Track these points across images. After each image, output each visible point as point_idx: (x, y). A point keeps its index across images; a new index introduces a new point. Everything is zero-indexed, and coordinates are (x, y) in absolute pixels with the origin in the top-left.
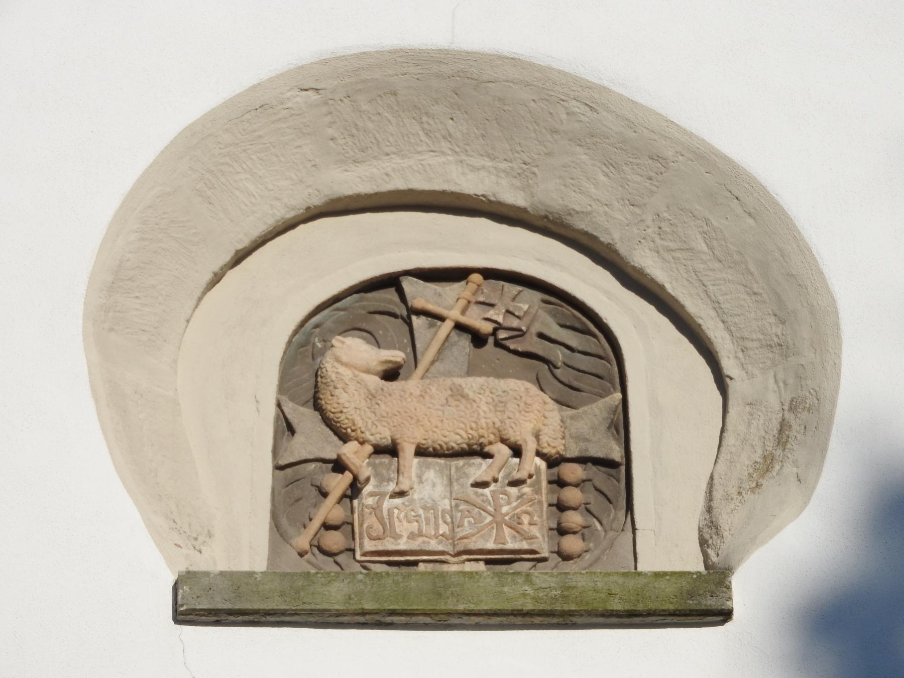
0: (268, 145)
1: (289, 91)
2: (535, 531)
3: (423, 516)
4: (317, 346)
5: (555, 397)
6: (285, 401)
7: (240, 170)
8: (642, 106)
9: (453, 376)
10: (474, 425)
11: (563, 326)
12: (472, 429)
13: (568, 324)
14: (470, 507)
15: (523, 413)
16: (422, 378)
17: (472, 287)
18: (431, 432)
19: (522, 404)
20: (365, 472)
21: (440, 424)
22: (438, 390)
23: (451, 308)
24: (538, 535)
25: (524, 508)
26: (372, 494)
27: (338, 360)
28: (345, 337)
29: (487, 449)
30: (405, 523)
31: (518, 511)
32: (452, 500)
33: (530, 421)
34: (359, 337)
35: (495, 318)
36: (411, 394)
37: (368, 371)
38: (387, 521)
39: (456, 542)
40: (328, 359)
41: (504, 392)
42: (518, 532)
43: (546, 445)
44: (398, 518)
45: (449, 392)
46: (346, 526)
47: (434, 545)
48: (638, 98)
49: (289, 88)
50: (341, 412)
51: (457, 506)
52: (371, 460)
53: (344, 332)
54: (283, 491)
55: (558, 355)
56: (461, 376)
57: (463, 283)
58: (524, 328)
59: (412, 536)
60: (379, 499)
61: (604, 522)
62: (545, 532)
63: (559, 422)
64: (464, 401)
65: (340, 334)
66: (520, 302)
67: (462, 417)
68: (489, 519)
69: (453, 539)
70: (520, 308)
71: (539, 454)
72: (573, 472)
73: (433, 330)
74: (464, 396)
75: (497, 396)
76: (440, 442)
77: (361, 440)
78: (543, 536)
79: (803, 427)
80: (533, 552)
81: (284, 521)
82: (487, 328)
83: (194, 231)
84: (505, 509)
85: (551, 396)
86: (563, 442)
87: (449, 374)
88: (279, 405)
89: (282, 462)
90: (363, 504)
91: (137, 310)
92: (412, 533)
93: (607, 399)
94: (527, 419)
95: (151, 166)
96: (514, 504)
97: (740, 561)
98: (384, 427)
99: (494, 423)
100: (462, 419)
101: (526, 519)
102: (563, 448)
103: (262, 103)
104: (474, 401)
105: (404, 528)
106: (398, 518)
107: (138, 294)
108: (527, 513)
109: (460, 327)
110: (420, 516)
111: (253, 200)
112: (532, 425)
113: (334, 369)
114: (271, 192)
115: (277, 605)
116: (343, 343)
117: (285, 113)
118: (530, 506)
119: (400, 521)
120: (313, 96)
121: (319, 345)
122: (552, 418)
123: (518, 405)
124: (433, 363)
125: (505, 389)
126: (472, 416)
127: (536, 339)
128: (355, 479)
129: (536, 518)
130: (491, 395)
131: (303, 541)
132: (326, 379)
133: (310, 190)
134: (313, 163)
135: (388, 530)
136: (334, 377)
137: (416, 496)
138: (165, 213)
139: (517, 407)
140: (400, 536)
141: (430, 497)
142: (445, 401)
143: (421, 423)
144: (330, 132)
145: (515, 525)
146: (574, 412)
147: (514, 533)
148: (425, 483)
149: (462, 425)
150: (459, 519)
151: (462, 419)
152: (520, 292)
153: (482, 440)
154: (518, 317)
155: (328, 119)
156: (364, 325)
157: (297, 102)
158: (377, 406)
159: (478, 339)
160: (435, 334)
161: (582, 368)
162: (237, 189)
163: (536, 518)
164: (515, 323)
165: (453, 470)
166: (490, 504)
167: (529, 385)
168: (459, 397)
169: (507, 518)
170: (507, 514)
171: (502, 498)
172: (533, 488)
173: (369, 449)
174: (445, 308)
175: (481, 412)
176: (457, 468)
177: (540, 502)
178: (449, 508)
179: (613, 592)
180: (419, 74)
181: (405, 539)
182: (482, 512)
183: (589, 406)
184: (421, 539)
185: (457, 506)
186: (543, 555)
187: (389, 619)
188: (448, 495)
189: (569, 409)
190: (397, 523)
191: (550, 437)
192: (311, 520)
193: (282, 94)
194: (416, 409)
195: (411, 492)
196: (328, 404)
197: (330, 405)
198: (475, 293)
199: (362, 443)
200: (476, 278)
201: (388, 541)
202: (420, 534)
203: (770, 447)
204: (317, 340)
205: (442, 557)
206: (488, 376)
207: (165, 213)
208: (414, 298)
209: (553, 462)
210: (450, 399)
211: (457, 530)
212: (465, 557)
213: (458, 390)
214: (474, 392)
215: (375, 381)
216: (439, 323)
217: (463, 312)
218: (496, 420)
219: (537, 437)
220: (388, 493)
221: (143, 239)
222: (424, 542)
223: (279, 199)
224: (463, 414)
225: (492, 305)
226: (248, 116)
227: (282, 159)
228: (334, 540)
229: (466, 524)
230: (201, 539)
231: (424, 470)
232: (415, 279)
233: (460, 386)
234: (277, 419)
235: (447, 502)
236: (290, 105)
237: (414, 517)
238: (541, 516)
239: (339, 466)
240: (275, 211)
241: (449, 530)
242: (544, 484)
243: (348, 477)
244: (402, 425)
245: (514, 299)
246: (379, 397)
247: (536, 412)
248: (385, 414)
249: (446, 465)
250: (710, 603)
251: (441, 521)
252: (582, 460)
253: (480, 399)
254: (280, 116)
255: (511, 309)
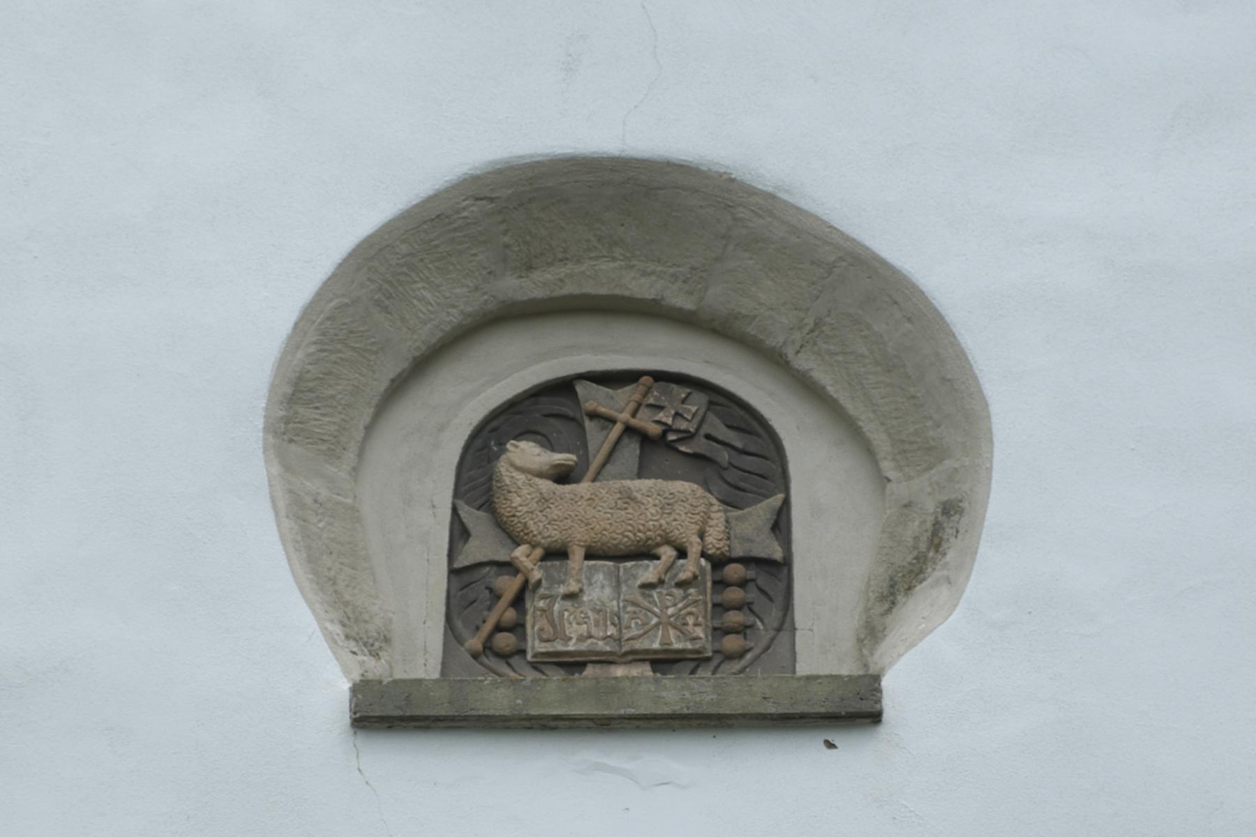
0: (445, 254)
1: (464, 200)
2: (699, 632)
3: (592, 618)
4: (494, 450)
5: (721, 498)
6: (461, 504)
7: (417, 279)
8: (806, 212)
9: (624, 479)
10: (641, 527)
11: (729, 427)
12: (639, 531)
13: (735, 425)
14: (637, 609)
15: (690, 515)
16: (594, 480)
17: (641, 389)
18: (600, 535)
19: (688, 506)
20: (537, 575)
21: (608, 526)
22: (608, 489)
23: (622, 411)
24: (702, 635)
25: (689, 609)
26: (543, 597)
27: (512, 465)
28: (518, 441)
29: (654, 552)
30: (574, 625)
31: (683, 612)
32: (620, 601)
33: (696, 523)
34: (534, 441)
35: (664, 420)
36: (582, 497)
37: (541, 475)
38: (557, 623)
39: (623, 643)
40: (503, 464)
41: (671, 494)
42: (682, 633)
43: (710, 546)
44: (568, 620)
45: (618, 495)
46: (518, 628)
47: (602, 646)
48: (804, 204)
49: (463, 197)
50: (514, 516)
51: (625, 607)
52: (544, 563)
53: (518, 437)
54: (460, 593)
55: (724, 456)
56: (632, 479)
57: (634, 386)
58: (692, 430)
59: (581, 639)
60: (550, 601)
61: (766, 621)
62: (709, 632)
63: (724, 523)
64: (632, 503)
65: (514, 439)
66: (690, 404)
67: (630, 519)
68: (655, 620)
69: (620, 640)
70: (689, 410)
71: (703, 555)
72: (734, 571)
73: (605, 432)
74: (634, 499)
75: (665, 498)
76: (609, 545)
77: (533, 543)
78: (707, 636)
79: (955, 530)
80: (697, 652)
81: (459, 624)
82: (654, 430)
83: (373, 340)
84: (670, 611)
85: (718, 496)
86: (728, 542)
87: (621, 476)
88: (455, 510)
89: (456, 565)
90: (535, 607)
91: (316, 420)
92: (581, 635)
93: (771, 500)
94: (692, 521)
95: (329, 279)
96: (680, 605)
97: (891, 664)
98: (555, 530)
99: (661, 525)
100: (631, 522)
101: (690, 620)
102: (727, 548)
103: (439, 213)
104: (643, 504)
105: (574, 630)
106: (568, 620)
107: (317, 405)
108: (690, 613)
109: (629, 430)
110: (588, 618)
111: (430, 308)
112: (698, 527)
113: (508, 473)
114: (449, 300)
115: (446, 712)
116: (517, 447)
117: (460, 222)
118: (695, 607)
119: (570, 623)
120: (490, 206)
121: (495, 449)
122: (718, 519)
123: (685, 507)
124: (604, 465)
125: (672, 491)
126: (639, 519)
127: (704, 440)
128: (526, 582)
129: (700, 619)
130: (659, 497)
131: (475, 642)
132: (501, 483)
133: (486, 297)
134: (488, 270)
135: (559, 633)
136: (507, 481)
137: (585, 598)
138: (344, 324)
139: (682, 508)
140: (570, 639)
141: (599, 599)
142: (614, 504)
143: (591, 526)
144: (506, 239)
145: (681, 628)
146: (740, 512)
147: (679, 633)
148: (595, 585)
149: (630, 528)
150: (626, 621)
151: (631, 522)
152: (689, 394)
153: (650, 542)
154: (687, 420)
155: (503, 227)
156: (539, 428)
157: (473, 211)
158: (548, 510)
159: (645, 439)
160: (608, 435)
161: (747, 468)
162: (415, 298)
163: (700, 619)
164: (683, 425)
165: (622, 570)
166: (656, 605)
167: (695, 486)
168: (628, 500)
169: (672, 619)
170: (672, 616)
171: (668, 599)
172: (697, 590)
173: (539, 552)
174: (617, 410)
175: (649, 514)
176: (625, 569)
177: (705, 603)
178: (616, 609)
179: (767, 696)
180: (591, 181)
181: (574, 641)
182: (649, 614)
183: (754, 507)
184: (589, 641)
185: (625, 607)
186: (706, 655)
187: (553, 724)
188: (616, 595)
189: (734, 509)
190: (567, 625)
191: (715, 539)
192: (484, 622)
193: (458, 203)
194: (586, 512)
195: (580, 594)
196: (502, 508)
197: (504, 510)
198: (645, 395)
199: (534, 547)
200: (646, 380)
201: (558, 643)
202: (590, 637)
203: (923, 546)
204: (492, 443)
205: (611, 658)
206: (657, 478)
207: (344, 324)
208: (587, 401)
209: (718, 562)
210: (619, 502)
211: (624, 631)
212: (630, 658)
213: (627, 492)
214: (643, 494)
215: (546, 485)
216: (610, 426)
217: (634, 415)
218: (663, 522)
219: (702, 535)
220: (558, 596)
221: (322, 351)
222: (592, 644)
223: (454, 306)
224: (630, 516)
225: (661, 408)
226: (425, 226)
227: (458, 267)
228: (505, 641)
229: (633, 625)
230: (377, 644)
231: (593, 572)
232: (589, 383)
233: (629, 489)
234: (452, 524)
235: (615, 603)
236: (465, 214)
237: (584, 618)
238: (705, 617)
239: (509, 567)
240: (452, 318)
241: (617, 631)
242: (709, 584)
243: (519, 580)
244: (573, 529)
245: (683, 401)
246: (551, 501)
247: (702, 514)
248: (556, 517)
249: (614, 566)
250: (865, 707)
251: (609, 623)
252: (746, 561)
253: (648, 501)
254: (456, 225)
255: (680, 411)
